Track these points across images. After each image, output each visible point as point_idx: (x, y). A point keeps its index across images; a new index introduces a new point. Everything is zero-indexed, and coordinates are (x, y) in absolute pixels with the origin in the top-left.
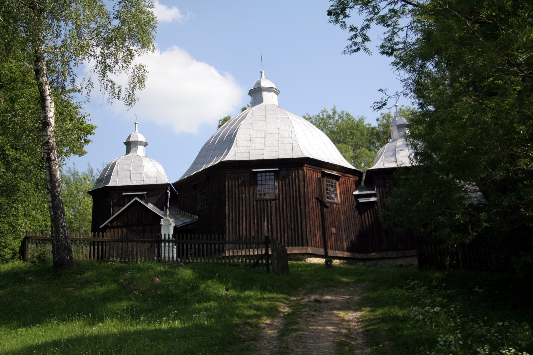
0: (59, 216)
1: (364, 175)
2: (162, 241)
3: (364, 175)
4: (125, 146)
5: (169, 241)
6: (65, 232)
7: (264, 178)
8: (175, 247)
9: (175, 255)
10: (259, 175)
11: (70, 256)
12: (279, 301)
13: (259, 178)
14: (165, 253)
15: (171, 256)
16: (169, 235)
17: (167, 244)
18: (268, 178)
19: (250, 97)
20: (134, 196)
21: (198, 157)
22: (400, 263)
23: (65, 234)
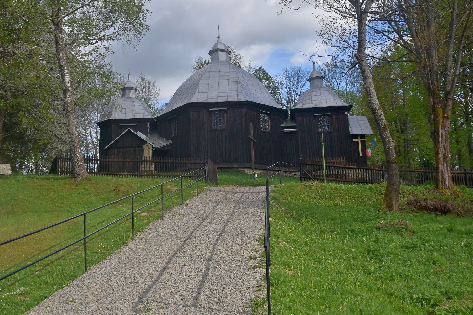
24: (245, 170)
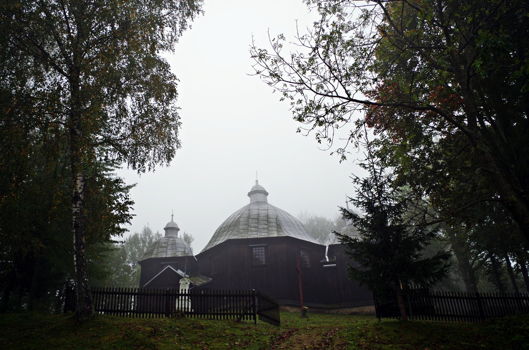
0: (82, 273)
1: (327, 248)
2: (179, 295)
3: (327, 248)
4: (164, 231)
5: (185, 295)
6: (87, 286)
8: (190, 300)
9: (190, 307)
10: (254, 249)
11: (90, 306)
12: (473, 29)
14: (485, 308)
15: (186, 307)
16: (185, 290)
17: (183, 297)
19: (249, 198)
20: (167, 265)
21: (213, 237)
22: (354, 311)
23: (87, 288)
24: (288, 308)
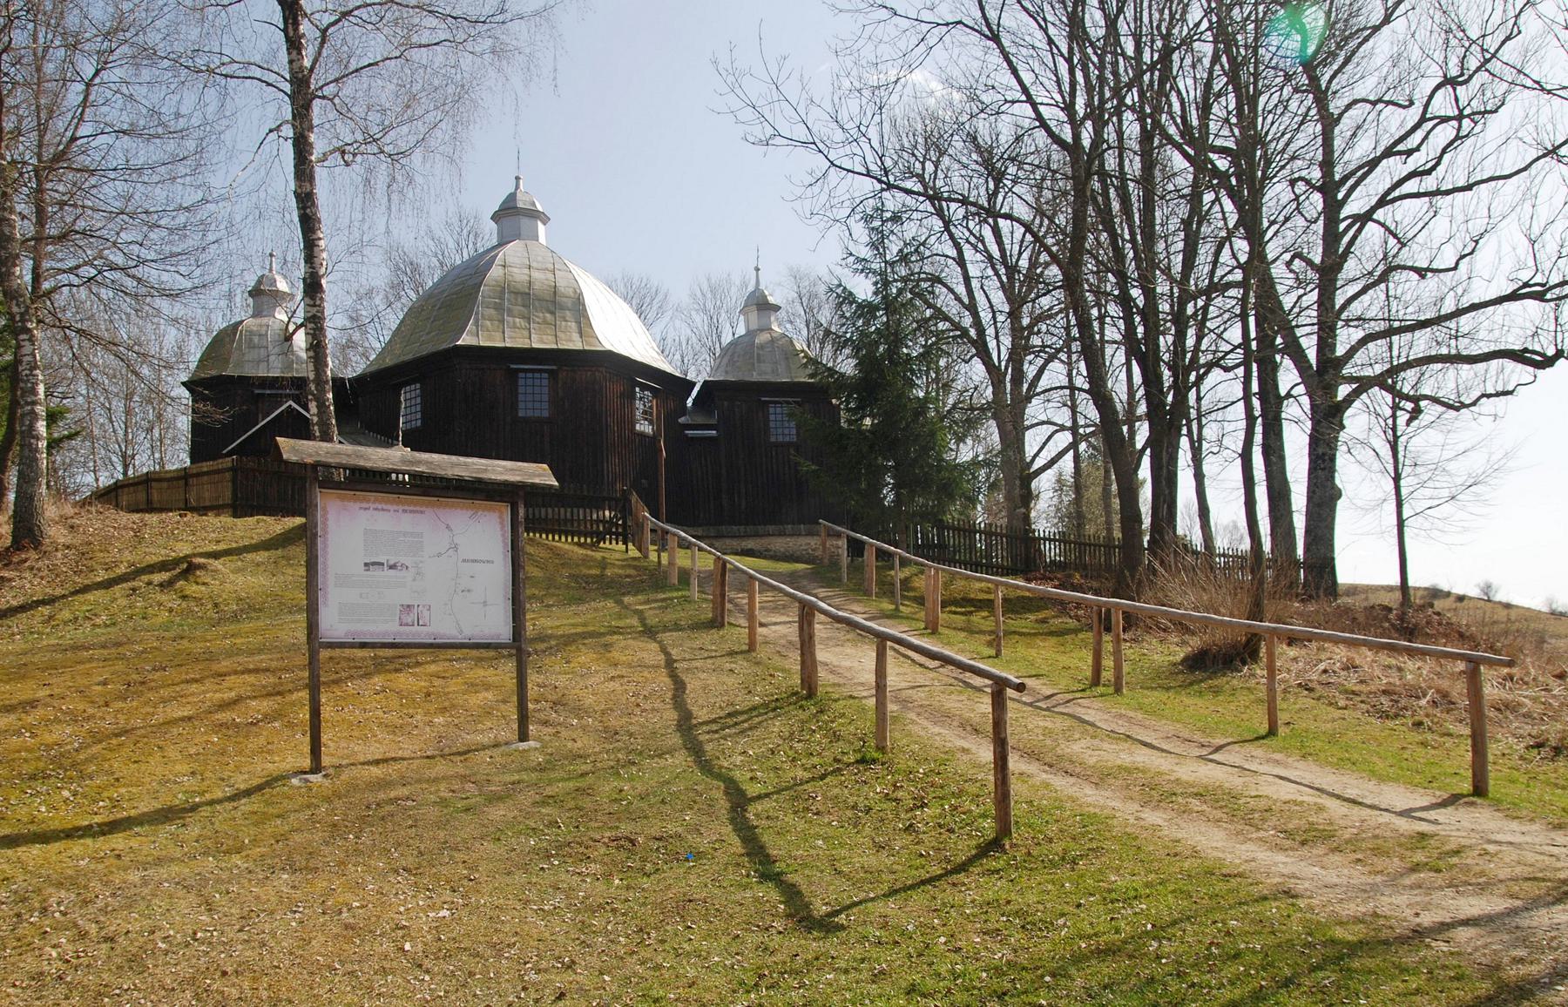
7: (530, 382)
10: (521, 375)
13: (521, 382)
18: (537, 382)
